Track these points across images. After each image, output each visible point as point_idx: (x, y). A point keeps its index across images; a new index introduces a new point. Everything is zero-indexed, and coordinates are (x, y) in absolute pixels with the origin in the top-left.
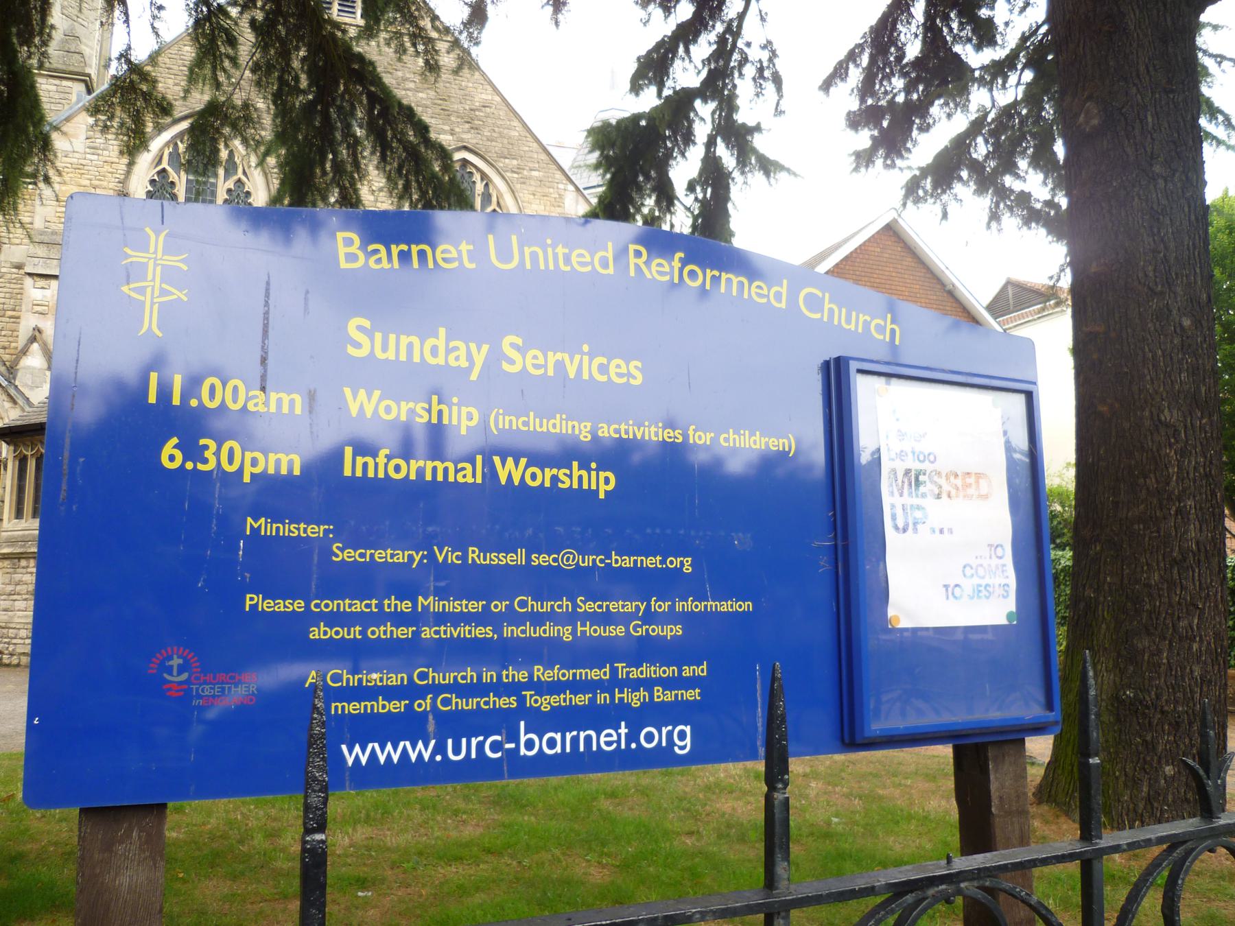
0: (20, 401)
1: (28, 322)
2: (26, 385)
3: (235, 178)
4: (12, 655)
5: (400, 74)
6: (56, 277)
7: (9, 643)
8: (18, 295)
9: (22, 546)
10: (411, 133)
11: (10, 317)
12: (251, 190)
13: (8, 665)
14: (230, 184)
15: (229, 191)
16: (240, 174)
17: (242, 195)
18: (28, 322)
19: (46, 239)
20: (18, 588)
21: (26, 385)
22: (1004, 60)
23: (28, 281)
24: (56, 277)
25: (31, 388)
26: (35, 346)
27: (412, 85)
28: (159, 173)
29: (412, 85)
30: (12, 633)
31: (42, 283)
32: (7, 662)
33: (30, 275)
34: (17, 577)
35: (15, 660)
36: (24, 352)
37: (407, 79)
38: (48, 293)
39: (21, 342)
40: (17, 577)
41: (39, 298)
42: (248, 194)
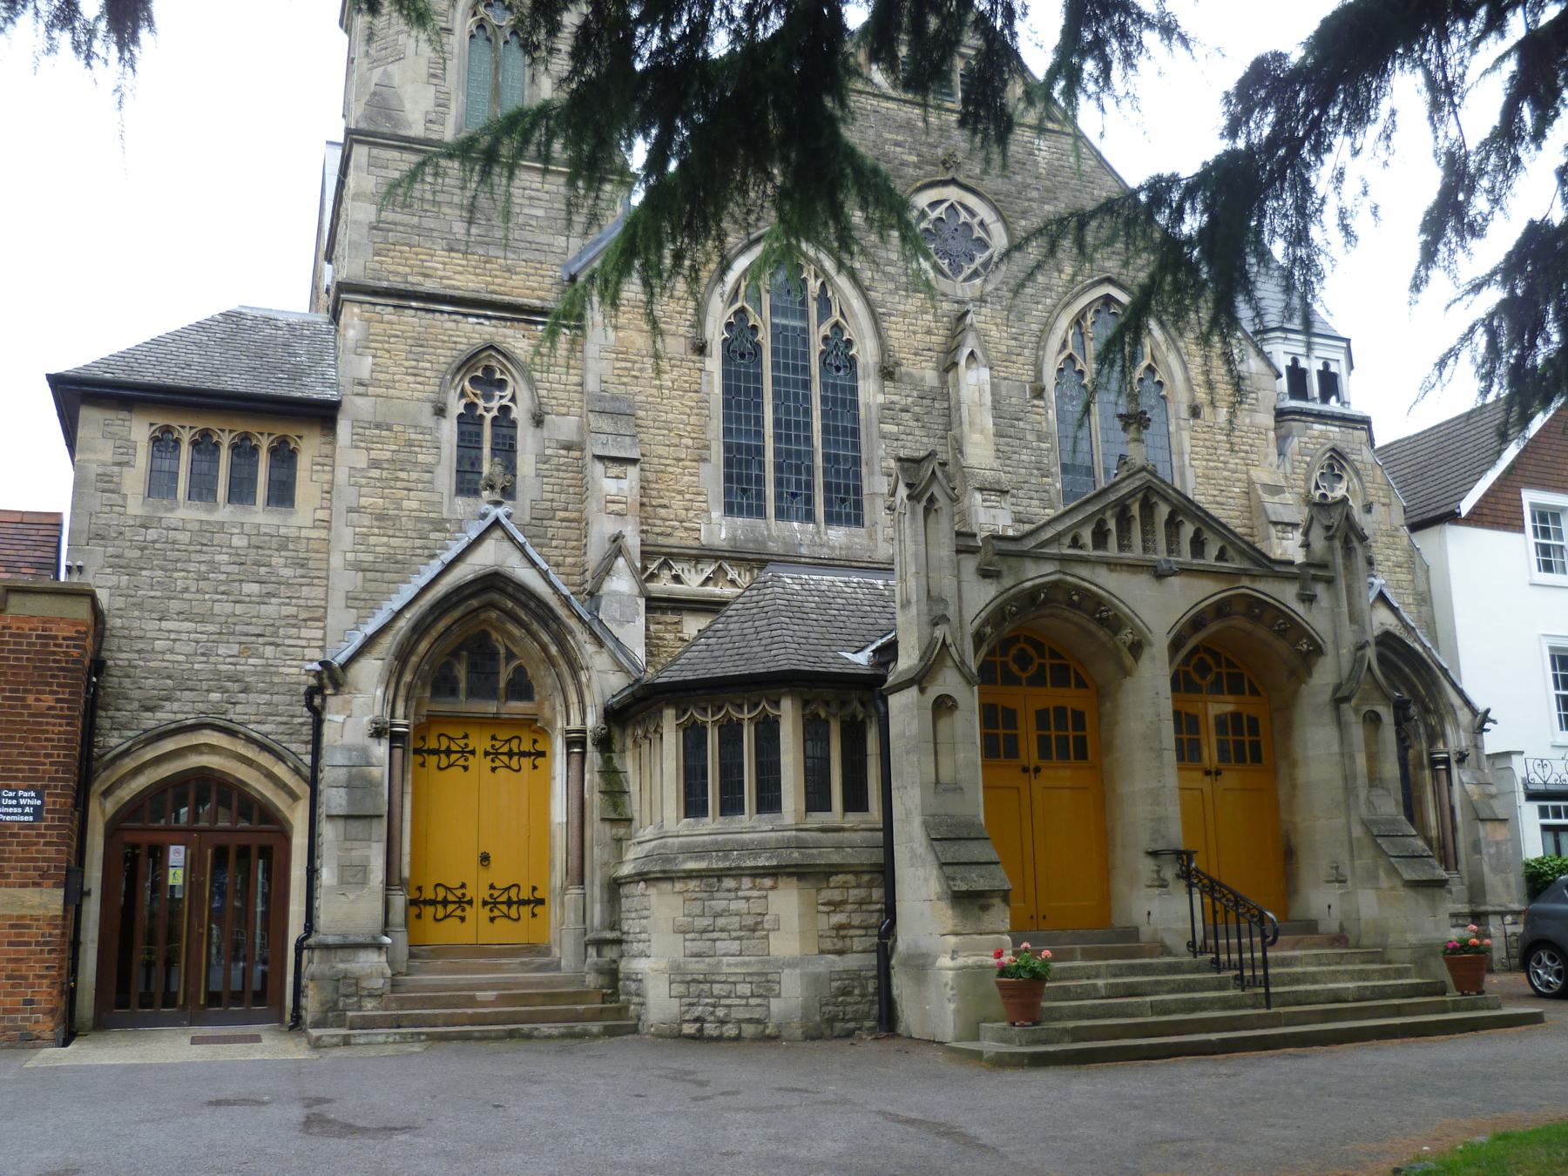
0: (610, 644)
1: (603, 528)
2: (613, 619)
3: (832, 320)
4: (722, 1022)
5: (1019, 178)
6: (634, 461)
7: (714, 1006)
8: (582, 489)
9: (719, 859)
10: (1205, 269)
11: (562, 520)
12: (854, 338)
13: (719, 1038)
14: (825, 329)
15: (825, 339)
16: (836, 315)
17: (842, 346)
18: (603, 528)
19: (608, 407)
20: (721, 922)
21: (613, 619)
22: (1076, 127)
23: (599, 468)
24: (634, 461)
25: (621, 624)
26: (621, 561)
27: (1035, 194)
28: (736, 313)
29: (1035, 194)
30: (717, 989)
31: (615, 470)
32: (715, 1033)
33: (600, 458)
34: (720, 905)
35: (730, 1030)
36: (606, 570)
37: (1028, 186)
38: (625, 484)
39: (594, 557)
40: (720, 905)
41: (614, 491)
42: (849, 343)
